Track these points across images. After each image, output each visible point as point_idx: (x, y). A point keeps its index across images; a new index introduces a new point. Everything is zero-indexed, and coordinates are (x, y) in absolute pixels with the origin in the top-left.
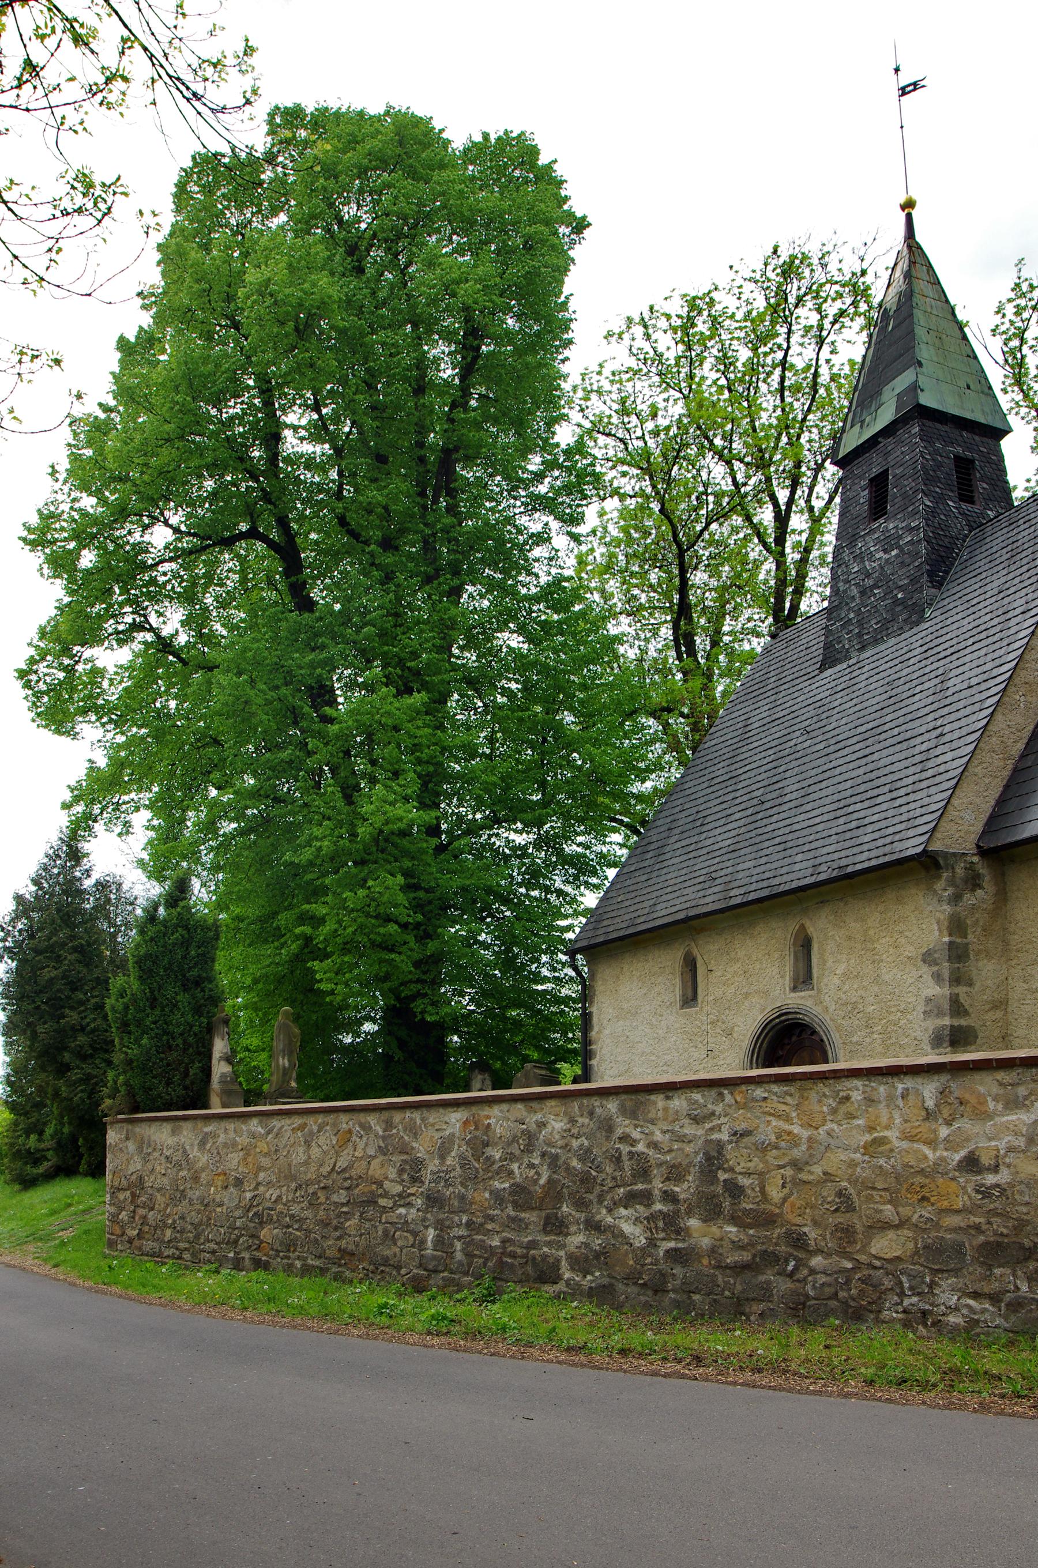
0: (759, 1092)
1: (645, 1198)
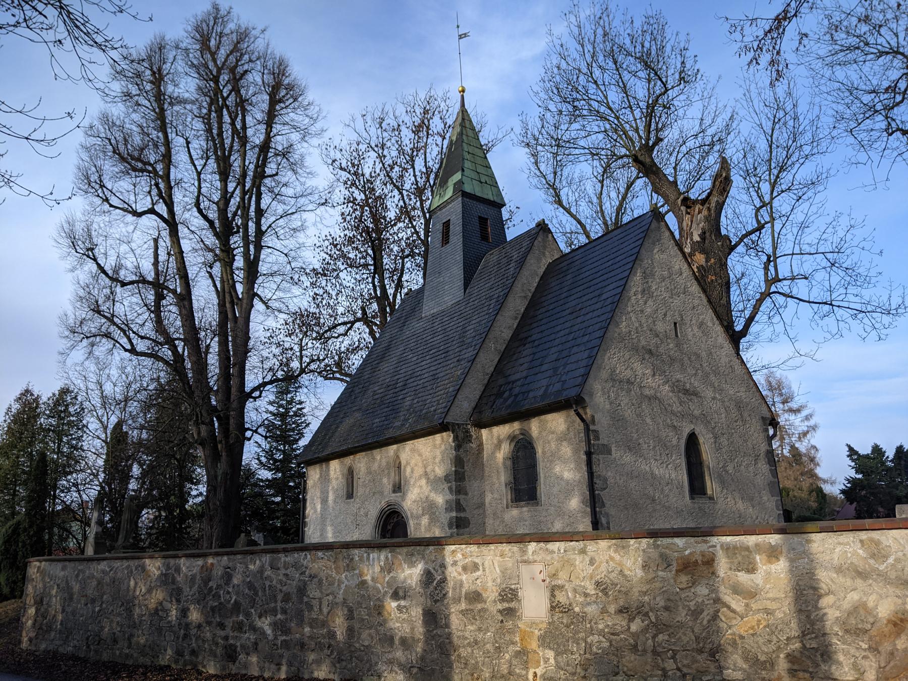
0: (320, 554)
1: (274, 612)
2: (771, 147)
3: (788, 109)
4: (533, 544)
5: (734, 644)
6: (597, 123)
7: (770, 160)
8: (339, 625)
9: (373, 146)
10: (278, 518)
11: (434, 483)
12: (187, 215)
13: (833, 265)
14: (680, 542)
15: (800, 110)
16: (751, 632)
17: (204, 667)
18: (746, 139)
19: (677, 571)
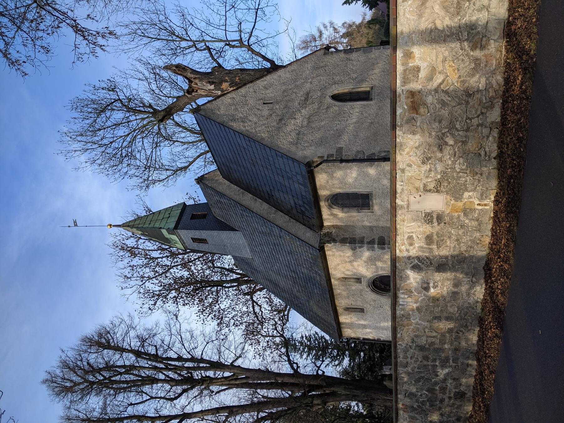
0: (399, 335)
1: (434, 366)
2: (159, 39)
3: (136, 27)
4: (397, 201)
5: (463, 82)
6: (137, 143)
7: (167, 40)
8: (444, 325)
9: (142, 283)
10: (374, 355)
11: (356, 257)
12: (178, 407)
13: (233, 7)
14: (399, 111)
15: (137, 21)
16: (456, 71)
17: (467, 413)
18: (152, 53)
19: (417, 114)
